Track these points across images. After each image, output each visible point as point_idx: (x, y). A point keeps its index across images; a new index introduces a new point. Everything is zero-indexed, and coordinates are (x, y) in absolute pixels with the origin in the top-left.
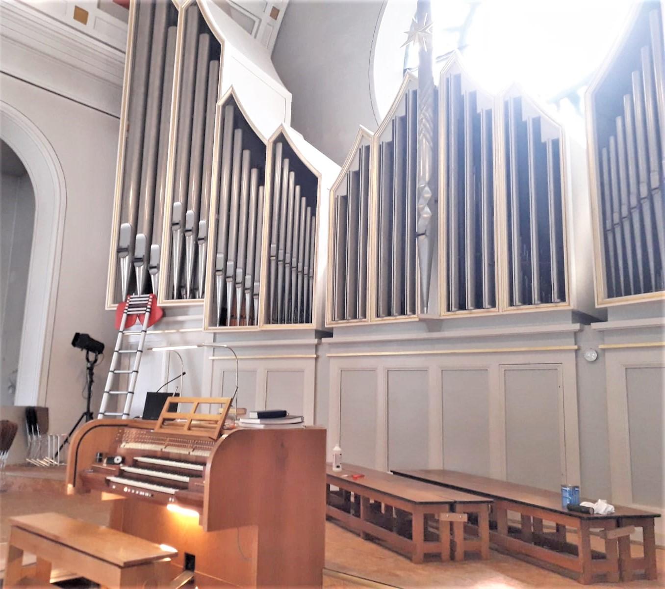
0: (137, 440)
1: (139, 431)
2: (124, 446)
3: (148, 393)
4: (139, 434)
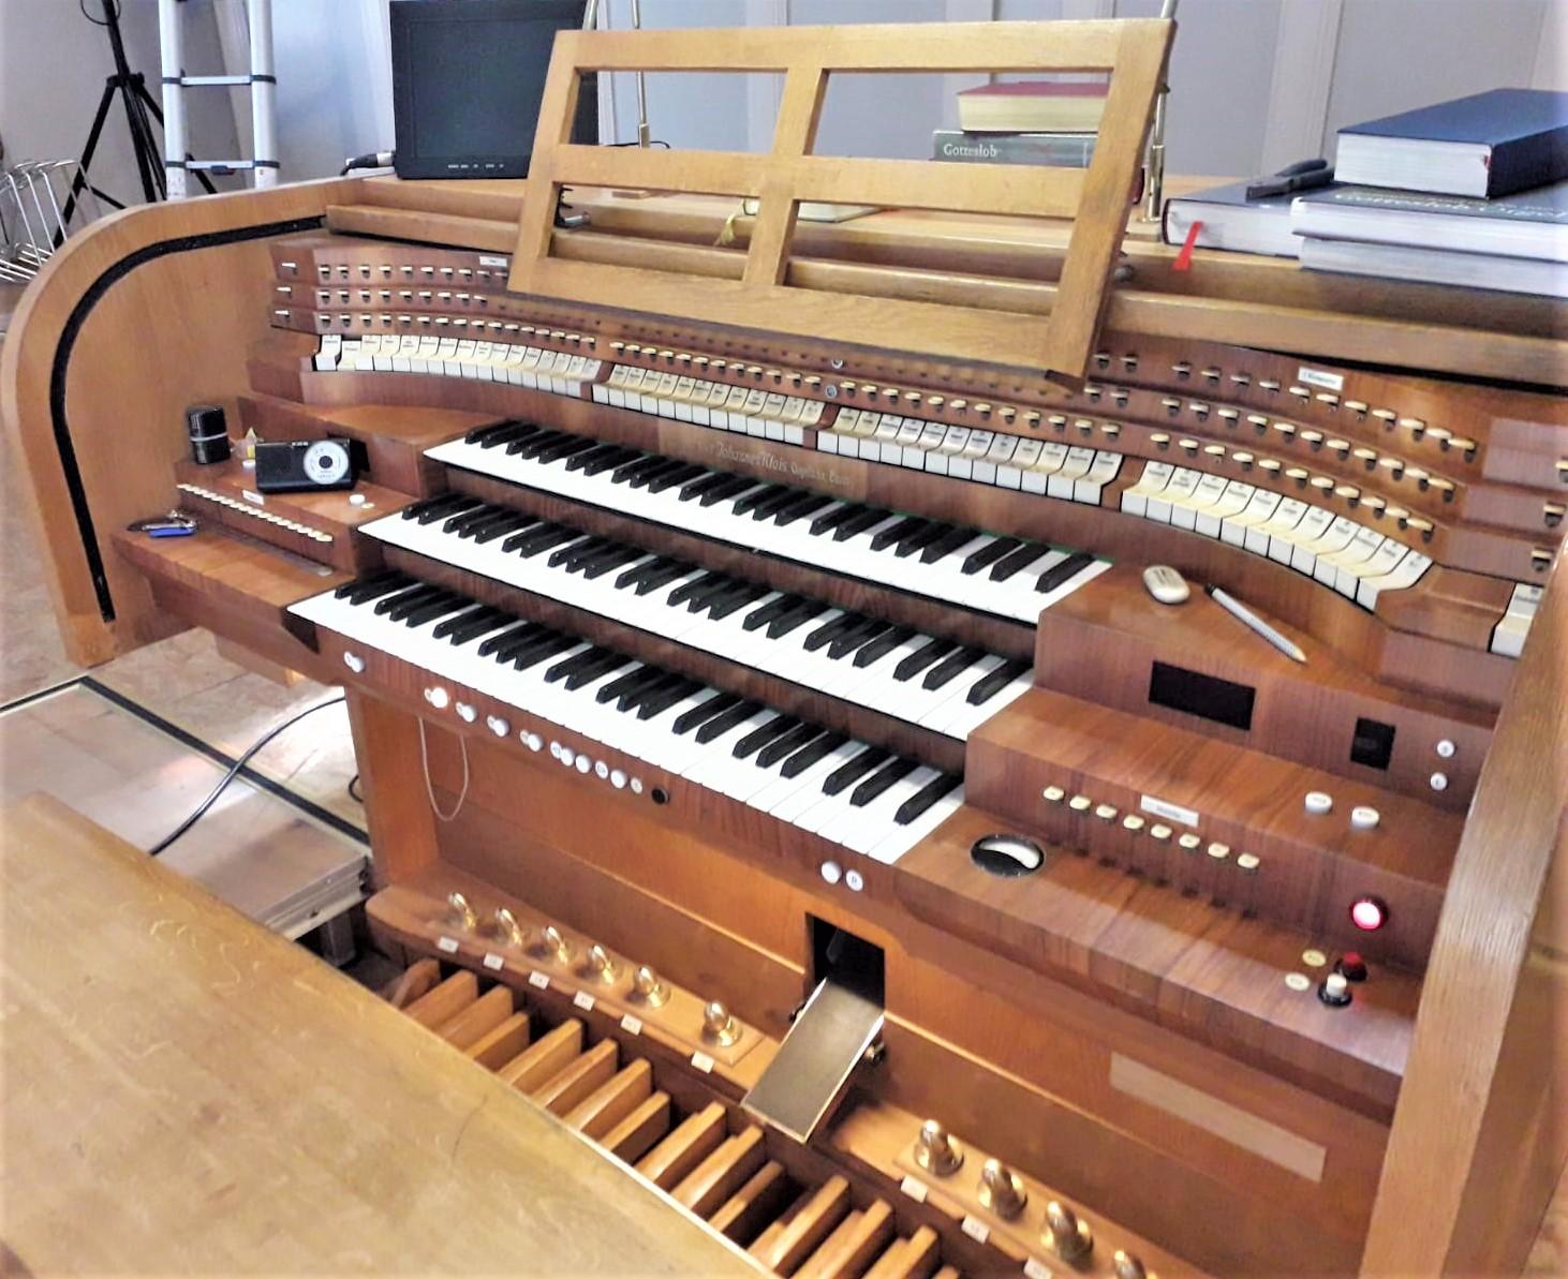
0: (407, 317)
1: (403, 262)
2: (338, 359)
4: (411, 280)
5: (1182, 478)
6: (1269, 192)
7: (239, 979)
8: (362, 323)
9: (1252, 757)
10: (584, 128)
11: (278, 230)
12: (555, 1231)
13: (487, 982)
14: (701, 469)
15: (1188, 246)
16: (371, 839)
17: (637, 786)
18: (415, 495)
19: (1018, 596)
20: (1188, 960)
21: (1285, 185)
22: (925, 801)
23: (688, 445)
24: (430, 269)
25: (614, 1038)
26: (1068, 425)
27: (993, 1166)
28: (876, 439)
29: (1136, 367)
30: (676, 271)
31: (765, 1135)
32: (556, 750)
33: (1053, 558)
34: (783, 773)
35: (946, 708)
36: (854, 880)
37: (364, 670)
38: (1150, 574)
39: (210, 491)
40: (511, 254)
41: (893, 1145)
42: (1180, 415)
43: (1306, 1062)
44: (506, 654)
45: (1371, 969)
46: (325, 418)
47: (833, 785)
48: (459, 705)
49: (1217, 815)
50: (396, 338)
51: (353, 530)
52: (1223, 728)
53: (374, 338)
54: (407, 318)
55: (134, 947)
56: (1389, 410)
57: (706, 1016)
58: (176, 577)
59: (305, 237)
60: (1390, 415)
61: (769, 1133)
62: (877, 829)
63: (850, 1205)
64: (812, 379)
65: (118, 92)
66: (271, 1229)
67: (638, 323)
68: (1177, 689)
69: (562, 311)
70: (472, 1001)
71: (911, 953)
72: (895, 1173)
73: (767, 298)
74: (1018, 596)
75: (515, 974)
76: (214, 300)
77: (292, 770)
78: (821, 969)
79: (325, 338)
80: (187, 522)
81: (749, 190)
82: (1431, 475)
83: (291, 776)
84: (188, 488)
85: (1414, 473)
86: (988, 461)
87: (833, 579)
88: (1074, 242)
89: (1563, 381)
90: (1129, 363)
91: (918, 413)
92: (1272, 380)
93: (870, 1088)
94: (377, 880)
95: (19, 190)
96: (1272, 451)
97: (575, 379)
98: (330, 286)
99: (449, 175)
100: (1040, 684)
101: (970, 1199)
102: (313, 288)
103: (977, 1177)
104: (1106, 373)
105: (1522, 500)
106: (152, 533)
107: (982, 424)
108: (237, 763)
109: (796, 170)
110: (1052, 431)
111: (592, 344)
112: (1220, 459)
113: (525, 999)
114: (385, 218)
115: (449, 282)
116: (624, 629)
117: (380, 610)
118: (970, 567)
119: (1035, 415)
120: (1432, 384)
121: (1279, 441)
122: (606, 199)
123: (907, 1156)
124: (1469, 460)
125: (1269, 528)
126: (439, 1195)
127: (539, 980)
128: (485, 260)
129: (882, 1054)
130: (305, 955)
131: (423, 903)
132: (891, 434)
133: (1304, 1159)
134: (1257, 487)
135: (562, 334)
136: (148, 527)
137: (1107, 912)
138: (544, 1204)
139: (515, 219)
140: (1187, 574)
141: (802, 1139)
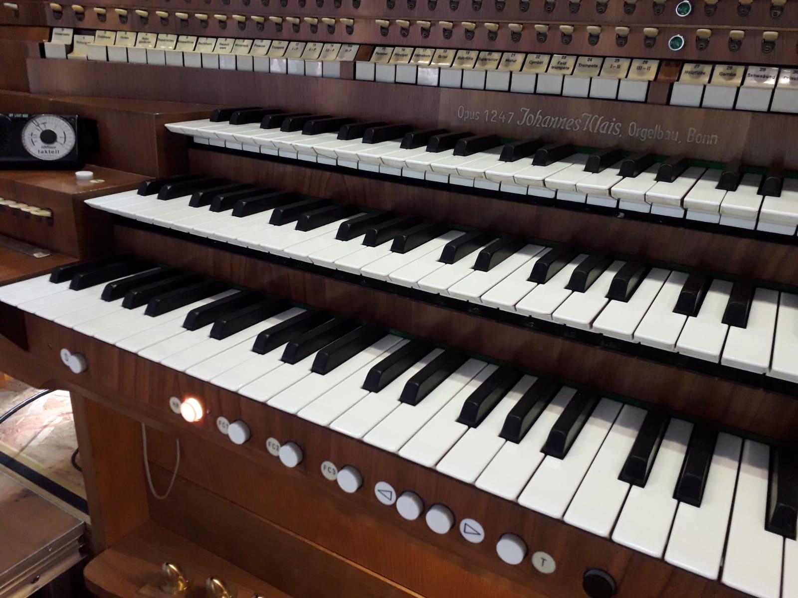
32: (384, 492)
48: (222, 420)
53: (108, 34)
77: (24, 445)
83: (22, 450)
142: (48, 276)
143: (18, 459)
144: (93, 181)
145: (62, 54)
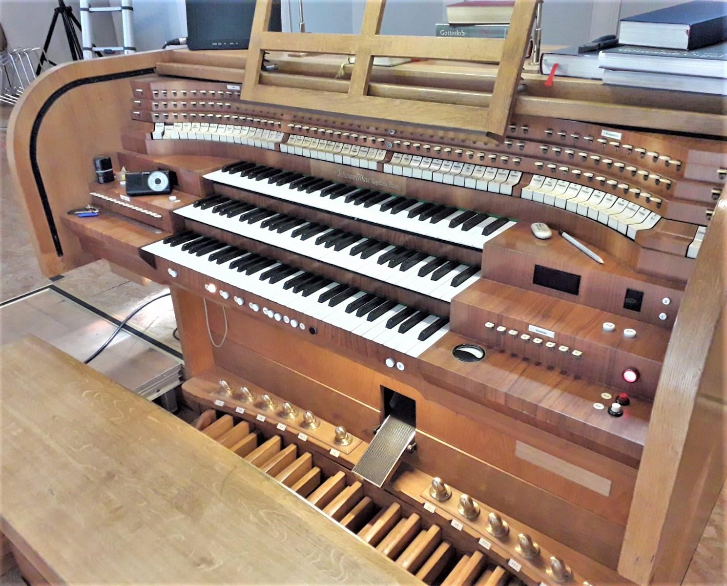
0: (194, 114)
1: (192, 88)
2: (163, 134)
3: (319, 302)
5: (549, 182)
6: (590, 49)
7: (123, 416)
8: (183, 118)
9: (579, 307)
10: (275, 24)
11: (134, 74)
12: (267, 524)
13: (237, 420)
14: (330, 183)
15: (552, 75)
16: (184, 357)
17: (302, 326)
18: (200, 197)
19: (475, 237)
20: (550, 398)
21: (596, 46)
22: (432, 330)
23: (324, 171)
24: (204, 92)
25: (295, 444)
26: (497, 159)
27: (465, 497)
28: (410, 167)
29: (526, 132)
30: (317, 90)
31: (363, 485)
33: (490, 220)
34: (368, 319)
35: (442, 289)
36: (400, 366)
37: (177, 276)
38: (534, 226)
39: (105, 196)
40: (241, 84)
41: (420, 488)
42: (525, 149)
43: (601, 441)
44: (242, 268)
45: (631, 400)
46: (157, 161)
47: (390, 324)
48: (221, 291)
49: (562, 333)
50: (189, 124)
51: (171, 212)
52: (566, 294)
54: (194, 115)
55: (74, 402)
56: (642, 148)
57: (337, 433)
58: (91, 235)
59: (146, 77)
60: (643, 151)
61: (365, 484)
62: (410, 343)
63: (401, 516)
64: (380, 140)
65: (60, 15)
66: (140, 525)
67: (301, 114)
68: (545, 277)
69: (265, 109)
70: (231, 428)
71: (426, 398)
72: (421, 501)
73: (359, 101)
74: (475, 237)
75: (250, 415)
76: (104, 106)
77: (147, 326)
78: (388, 411)
79: (156, 124)
80: (95, 210)
81: (350, 51)
82: (661, 178)
84: (95, 194)
85: (653, 176)
86: (461, 176)
87: (391, 231)
88: (499, 74)
89: (725, 134)
90: (525, 130)
91: (429, 155)
92: (589, 136)
93: (409, 463)
94: (187, 375)
95: (15, 62)
96: (588, 168)
97: (272, 142)
98: (158, 100)
99: (212, 48)
100: (484, 277)
101: (455, 511)
102: (150, 101)
103: (458, 502)
104: (515, 134)
105: (702, 188)
106: (79, 215)
107: (458, 159)
108: (121, 323)
109: (373, 42)
110: (490, 161)
111: (280, 125)
112: (565, 173)
113: (254, 427)
114: (183, 68)
115: (213, 97)
116: (296, 256)
117: (184, 249)
118: (453, 225)
119: (482, 155)
120: (661, 136)
121: (593, 164)
122: (285, 57)
123: (426, 493)
124: (678, 170)
125: (588, 204)
126: (214, 509)
127: (261, 418)
128: (229, 87)
129: (415, 448)
130: (155, 406)
131: (209, 385)
132: (417, 164)
133: (601, 486)
134: (583, 185)
135: (266, 121)
136: (77, 212)
137: (514, 377)
138: (262, 513)
139: (243, 68)
140: (551, 226)
141: (380, 487)
142: (163, 241)
143: (145, 333)
144: (176, 201)
145: (160, 137)
